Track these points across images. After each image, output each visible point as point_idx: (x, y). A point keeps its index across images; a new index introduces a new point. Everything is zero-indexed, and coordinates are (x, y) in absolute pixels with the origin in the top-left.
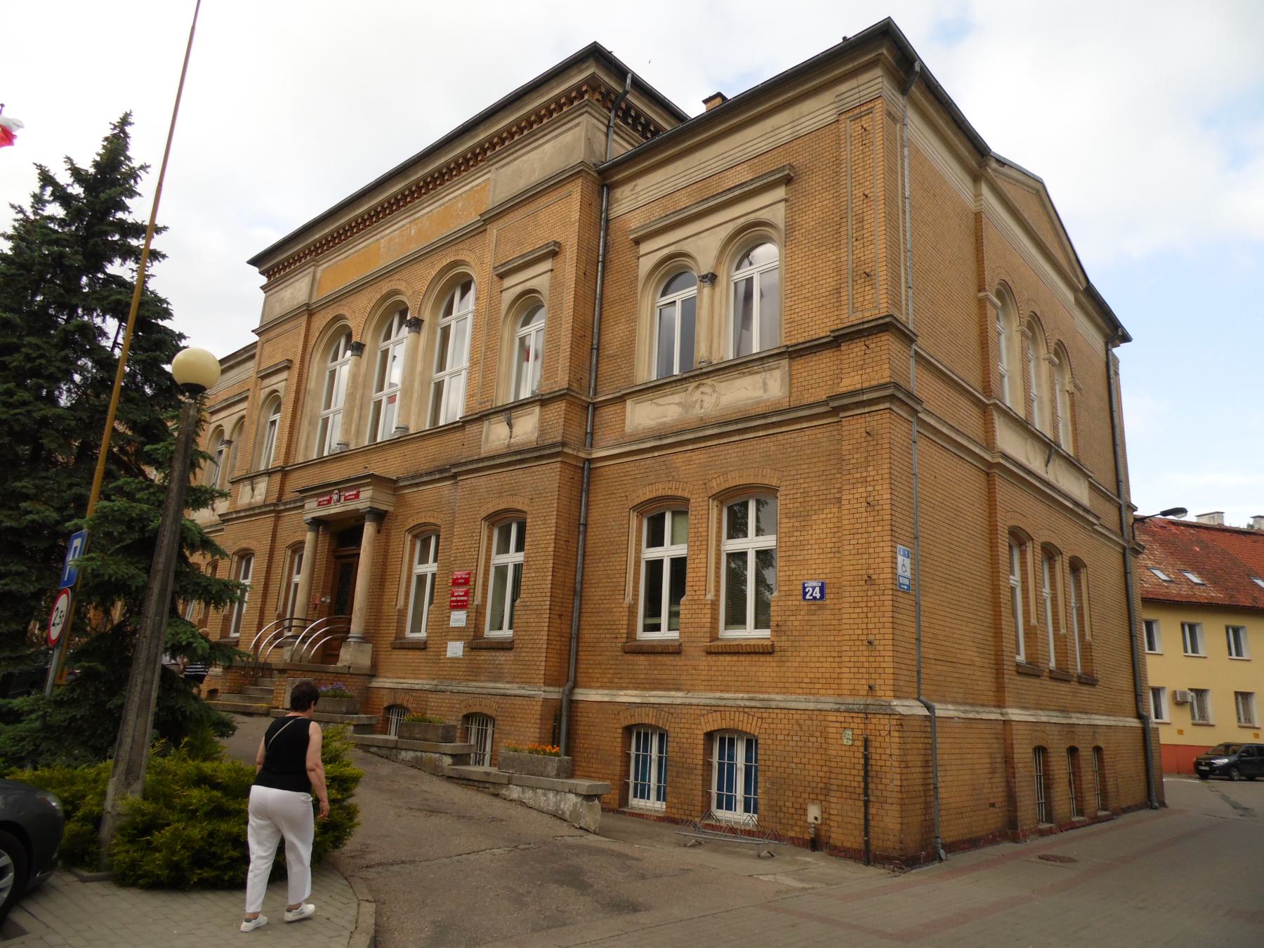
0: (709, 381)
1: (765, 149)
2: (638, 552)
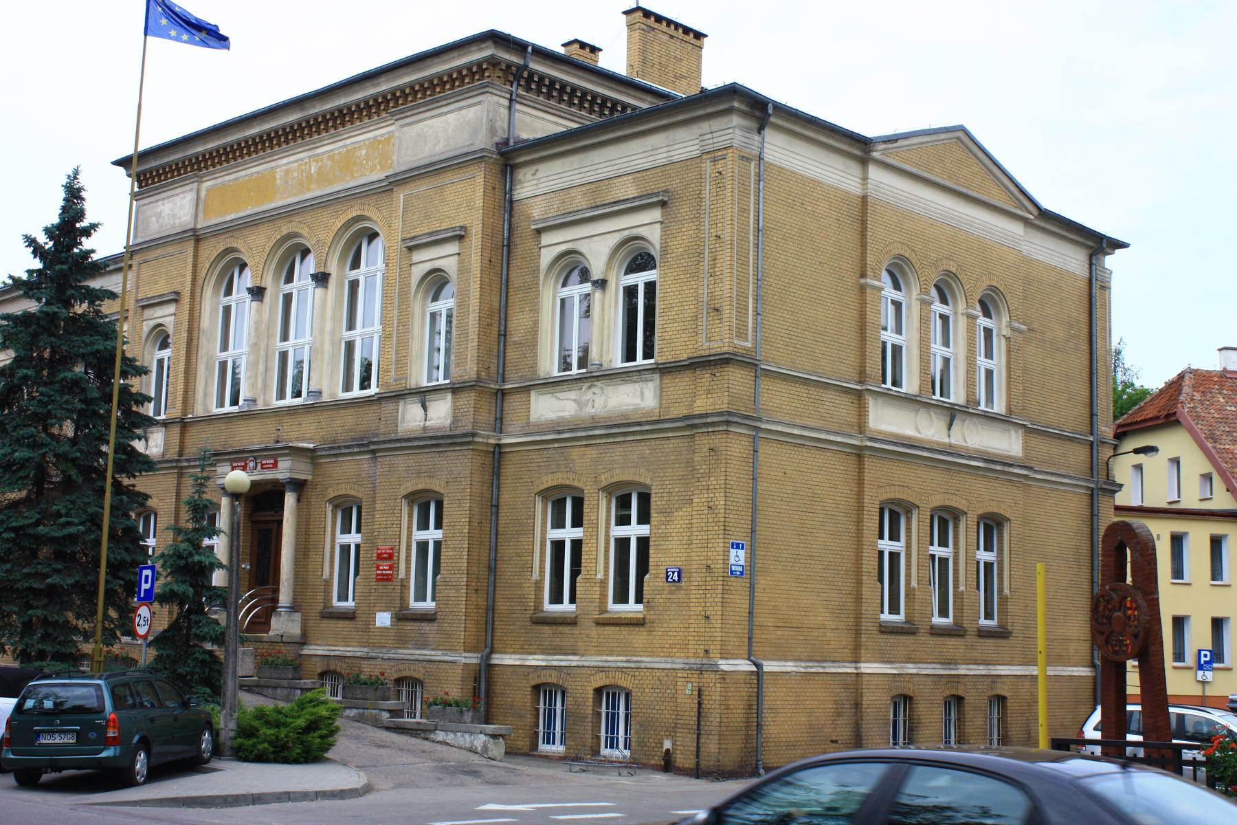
0: (598, 384)
1: (646, 166)
2: (544, 533)
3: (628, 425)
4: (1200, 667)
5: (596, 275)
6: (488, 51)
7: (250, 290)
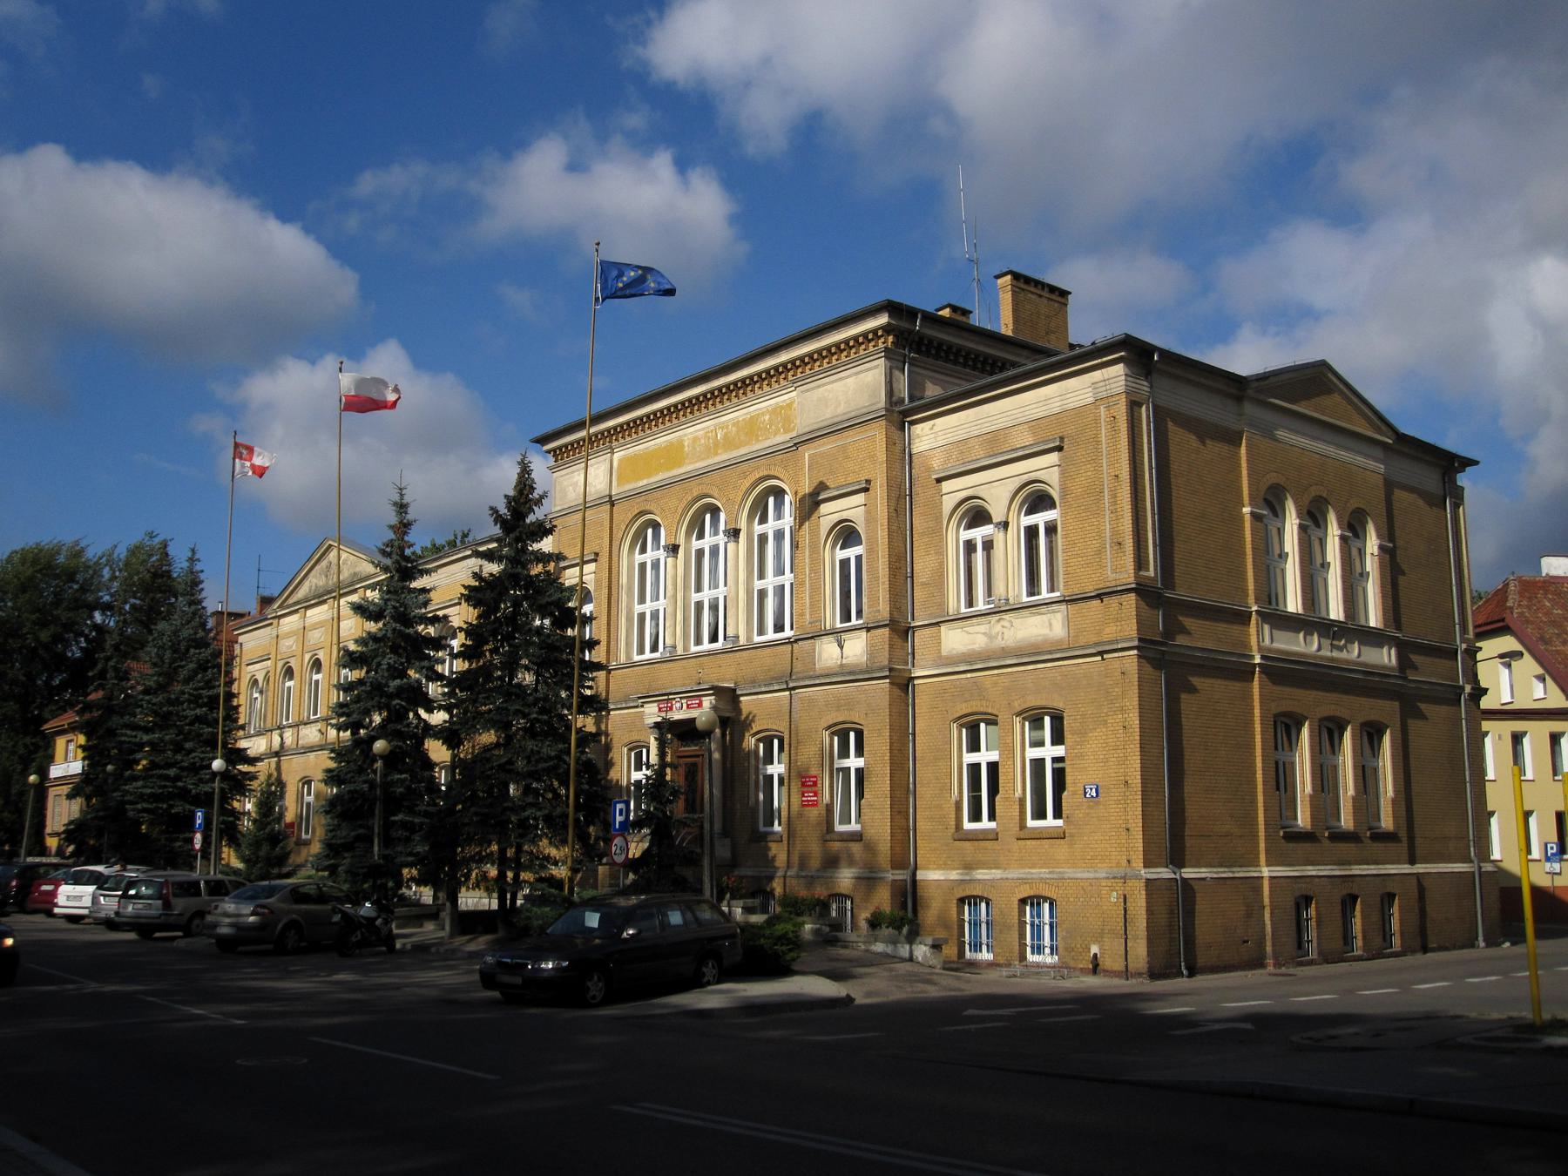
3: (1039, 653)
4: (1548, 859)
5: (997, 516)
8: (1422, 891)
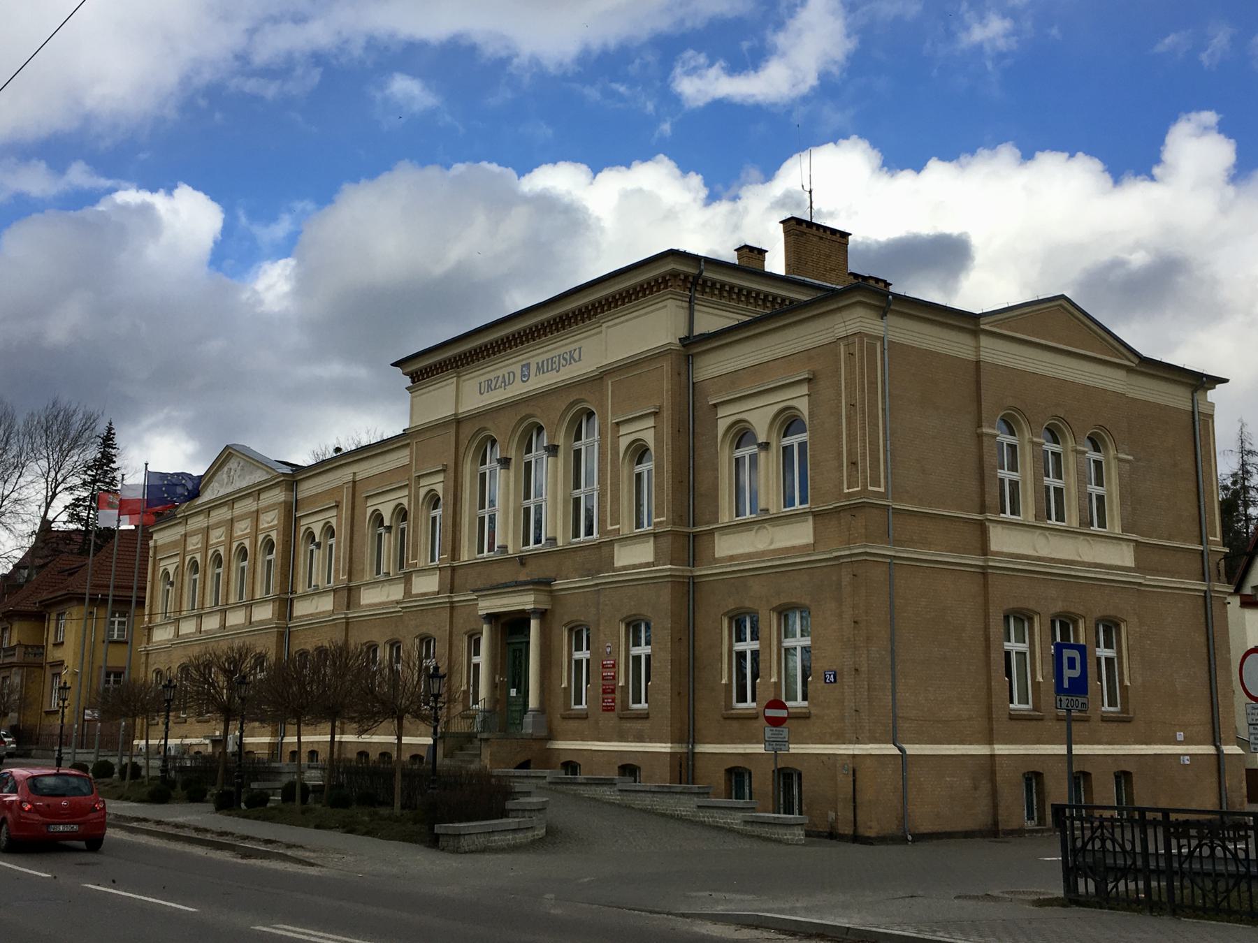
6: (670, 266)
7: (499, 461)
8: (993, 765)
